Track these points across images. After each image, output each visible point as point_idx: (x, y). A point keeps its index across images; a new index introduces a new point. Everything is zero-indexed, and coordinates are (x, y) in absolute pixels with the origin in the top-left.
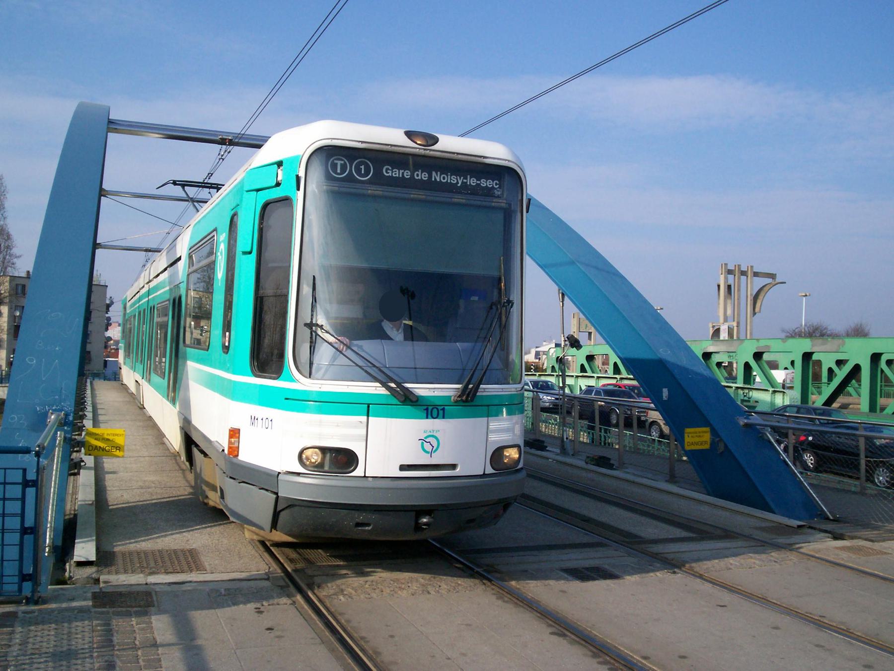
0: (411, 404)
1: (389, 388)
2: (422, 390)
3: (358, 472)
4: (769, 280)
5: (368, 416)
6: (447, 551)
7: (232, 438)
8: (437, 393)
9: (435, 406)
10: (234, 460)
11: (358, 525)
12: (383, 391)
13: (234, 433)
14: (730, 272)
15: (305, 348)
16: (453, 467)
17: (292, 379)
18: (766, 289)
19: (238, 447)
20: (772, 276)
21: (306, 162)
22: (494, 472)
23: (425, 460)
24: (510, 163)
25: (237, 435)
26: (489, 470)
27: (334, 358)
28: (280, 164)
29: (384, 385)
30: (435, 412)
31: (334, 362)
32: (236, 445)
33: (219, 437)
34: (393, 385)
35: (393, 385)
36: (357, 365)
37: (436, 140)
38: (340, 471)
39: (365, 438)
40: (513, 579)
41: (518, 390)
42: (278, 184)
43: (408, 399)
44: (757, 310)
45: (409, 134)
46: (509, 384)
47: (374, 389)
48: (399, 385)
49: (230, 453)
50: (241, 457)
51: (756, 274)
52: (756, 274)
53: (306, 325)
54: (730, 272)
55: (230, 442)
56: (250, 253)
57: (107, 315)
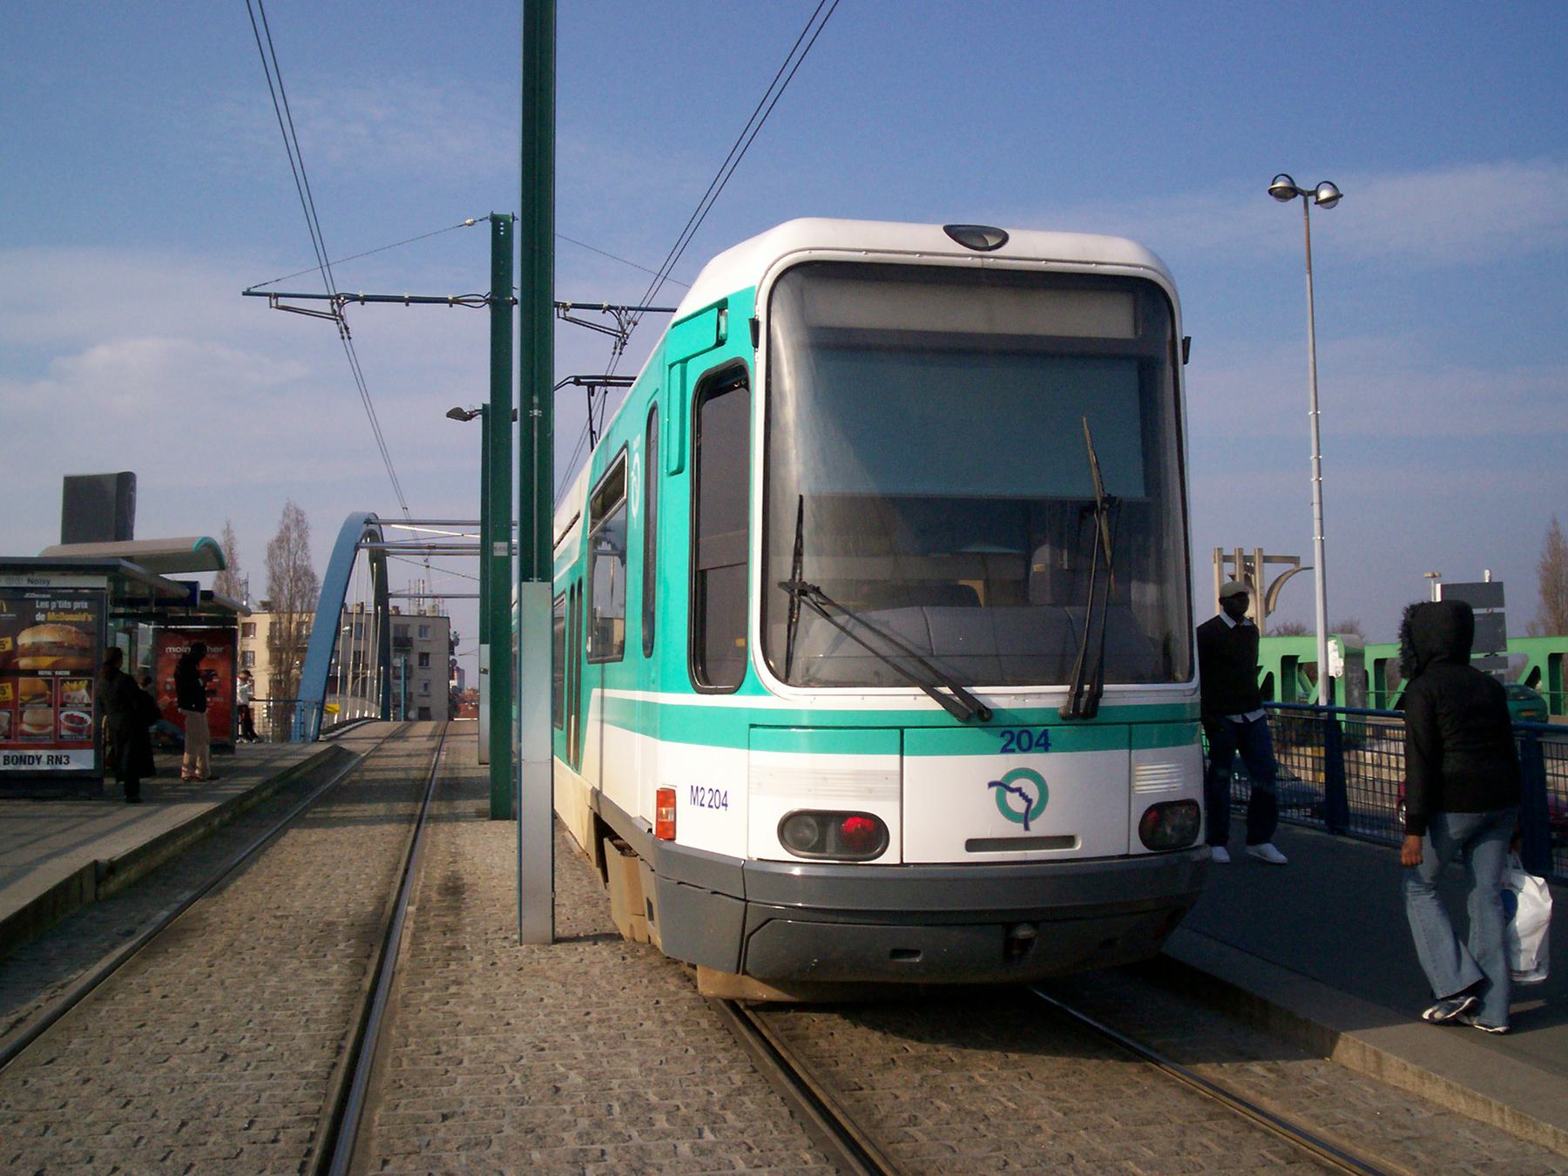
0: (981, 723)
1: (940, 698)
2: (1000, 697)
3: (890, 857)
4: (1291, 566)
5: (902, 754)
6: (1072, 1012)
7: (662, 806)
8: (1031, 703)
9: (1025, 729)
10: (667, 845)
11: (896, 953)
12: (930, 704)
13: (666, 798)
14: (1226, 559)
15: (779, 631)
16: (1068, 841)
17: (760, 690)
18: (1283, 578)
19: (674, 823)
20: (1294, 560)
21: (769, 289)
22: (1146, 850)
23: (1016, 830)
24: (1147, 271)
25: (672, 800)
26: (1138, 847)
27: (836, 644)
28: (722, 306)
29: (930, 690)
30: (1025, 740)
31: (833, 651)
32: (671, 818)
33: (640, 808)
34: (946, 690)
35: (946, 690)
36: (877, 654)
37: (1005, 239)
38: (860, 856)
39: (899, 795)
40: (1206, 1061)
41: (1187, 693)
42: (720, 342)
43: (977, 716)
44: (1271, 607)
45: (953, 232)
46: (1175, 681)
47: (910, 700)
48: (957, 690)
49: (659, 834)
50: (681, 840)
51: (1267, 559)
52: (1267, 559)
53: (782, 585)
54: (1226, 559)
55: (659, 815)
56: (680, 471)
57: (451, 658)
